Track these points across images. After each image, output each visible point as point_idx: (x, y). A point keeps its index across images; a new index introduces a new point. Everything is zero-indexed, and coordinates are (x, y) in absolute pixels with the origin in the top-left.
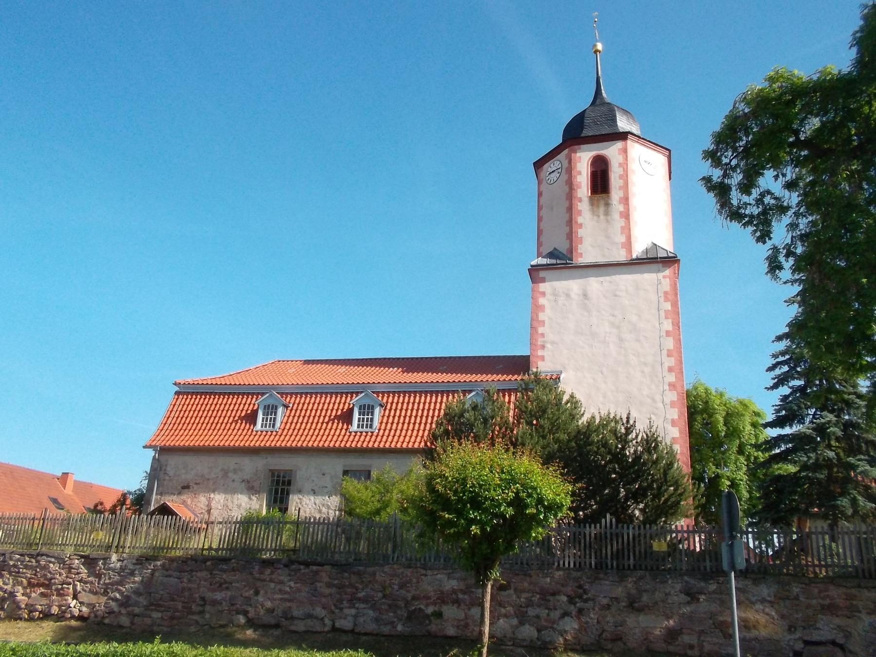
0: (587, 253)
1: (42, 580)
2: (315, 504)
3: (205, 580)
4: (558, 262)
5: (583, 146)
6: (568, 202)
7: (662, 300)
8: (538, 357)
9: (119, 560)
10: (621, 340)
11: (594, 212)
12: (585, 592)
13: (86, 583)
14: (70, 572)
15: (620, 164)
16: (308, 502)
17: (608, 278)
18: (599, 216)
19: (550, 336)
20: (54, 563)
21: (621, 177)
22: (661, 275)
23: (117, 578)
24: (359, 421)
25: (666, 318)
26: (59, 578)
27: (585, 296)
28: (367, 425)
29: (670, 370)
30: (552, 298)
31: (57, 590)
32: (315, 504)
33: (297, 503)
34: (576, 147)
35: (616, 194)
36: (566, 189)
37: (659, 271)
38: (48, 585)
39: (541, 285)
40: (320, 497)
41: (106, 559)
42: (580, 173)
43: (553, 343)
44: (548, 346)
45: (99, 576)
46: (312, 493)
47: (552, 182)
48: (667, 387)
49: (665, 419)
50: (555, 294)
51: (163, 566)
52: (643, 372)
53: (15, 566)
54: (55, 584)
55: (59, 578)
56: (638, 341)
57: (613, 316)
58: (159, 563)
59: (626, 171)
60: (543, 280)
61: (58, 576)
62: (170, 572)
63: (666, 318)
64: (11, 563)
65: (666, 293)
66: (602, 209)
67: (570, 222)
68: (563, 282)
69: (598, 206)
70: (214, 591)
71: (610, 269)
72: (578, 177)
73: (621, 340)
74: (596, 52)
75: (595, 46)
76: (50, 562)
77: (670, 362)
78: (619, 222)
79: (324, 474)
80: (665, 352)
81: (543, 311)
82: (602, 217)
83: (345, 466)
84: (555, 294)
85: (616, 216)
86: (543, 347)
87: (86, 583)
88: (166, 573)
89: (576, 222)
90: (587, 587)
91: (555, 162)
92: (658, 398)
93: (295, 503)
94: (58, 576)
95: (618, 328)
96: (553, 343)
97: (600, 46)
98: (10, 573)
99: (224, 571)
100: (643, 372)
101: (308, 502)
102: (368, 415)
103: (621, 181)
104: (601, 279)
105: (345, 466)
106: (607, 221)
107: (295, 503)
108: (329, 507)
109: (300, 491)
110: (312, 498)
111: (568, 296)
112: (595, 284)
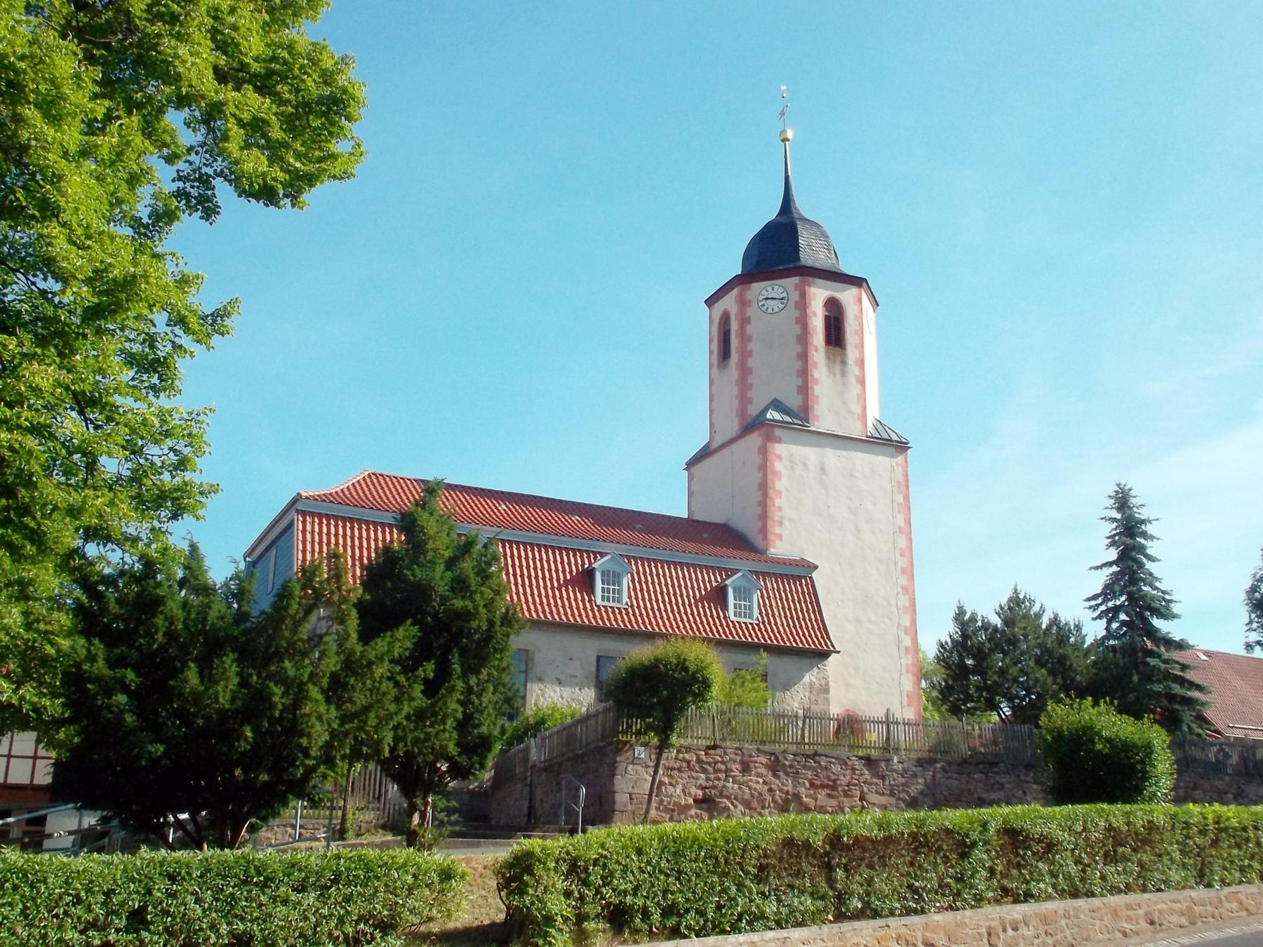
0: (824, 420)
1: (826, 781)
2: (562, 698)
3: (981, 782)
4: (796, 421)
5: (817, 280)
6: (748, 333)
7: (895, 490)
8: (775, 534)
9: (899, 762)
10: (858, 529)
11: (830, 367)
12: (1243, 791)
13: (870, 784)
14: (854, 773)
15: (855, 316)
16: (552, 694)
17: (844, 453)
18: (835, 375)
19: (788, 512)
20: (834, 764)
21: (856, 332)
22: (894, 461)
23: (902, 780)
24: (735, 607)
25: (899, 512)
26: (844, 780)
27: (823, 469)
28: (745, 613)
29: (903, 571)
30: (788, 464)
31: (844, 791)
32: (562, 698)
33: (537, 695)
34: (810, 279)
35: (851, 353)
36: (797, 329)
37: (892, 456)
38: (832, 786)
39: (777, 445)
40: (568, 689)
41: (888, 761)
42: (815, 314)
43: (790, 520)
44: (786, 523)
45: (883, 778)
46: (557, 683)
47: (770, 311)
48: (900, 590)
49: (899, 625)
50: (791, 460)
51: (942, 768)
52: (878, 569)
53: (791, 766)
54: (841, 785)
55: (844, 780)
56: (873, 532)
57: (850, 499)
58: (938, 766)
59: (861, 325)
60: (779, 440)
61: (842, 777)
62: (950, 774)
63: (899, 512)
64: (787, 763)
65: (899, 483)
66: (838, 367)
67: (804, 373)
68: (800, 448)
69: (834, 362)
70: (988, 791)
71: (840, 441)
72: (814, 319)
73: (858, 529)
74: (785, 140)
75: (784, 132)
76: (831, 763)
77: (902, 563)
78: (855, 389)
79: (571, 659)
80: (898, 551)
81: (780, 479)
82: (838, 377)
83: (599, 651)
84: (791, 460)
85: (852, 380)
86: (781, 524)
87: (870, 784)
88: (947, 776)
89: (812, 376)
90: (1243, 787)
91: (776, 287)
92: (893, 601)
93: (534, 696)
94: (842, 777)
95: (855, 514)
96: (790, 520)
97: (790, 134)
98: (787, 774)
99: (996, 773)
100: (878, 569)
101: (552, 694)
102: (614, 585)
103: (856, 337)
104: (839, 452)
105: (599, 651)
106: (843, 383)
107: (534, 696)
108: (581, 703)
109: (540, 680)
110: (557, 689)
111: (805, 465)
112: (833, 457)
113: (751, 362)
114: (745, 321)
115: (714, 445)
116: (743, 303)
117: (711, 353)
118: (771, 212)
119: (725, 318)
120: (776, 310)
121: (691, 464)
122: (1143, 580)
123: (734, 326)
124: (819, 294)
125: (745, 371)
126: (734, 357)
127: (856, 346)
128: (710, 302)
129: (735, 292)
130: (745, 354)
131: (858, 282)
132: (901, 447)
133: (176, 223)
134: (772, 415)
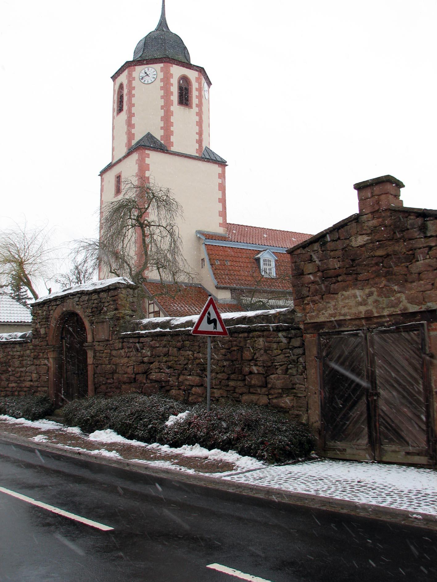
91: (150, 69)
113: (134, 110)
114: (131, 88)
115: (114, 161)
116: (130, 77)
117: (114, 103)
118: (152, 26)
119: (121, 86)
120: (150, 82)
121: (102, 173)
122: (420, 233)
123: (125, 91)
124: (177, 71)
125: (131, 115)
126: (125, 107)
127: (197, 89)
128: (114, 78)
129: (126, 73)
130: (131, 105)
131: (201, 70)
132: (222, 163)
133: (171, 196)
134: (434, 436)
